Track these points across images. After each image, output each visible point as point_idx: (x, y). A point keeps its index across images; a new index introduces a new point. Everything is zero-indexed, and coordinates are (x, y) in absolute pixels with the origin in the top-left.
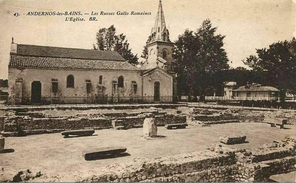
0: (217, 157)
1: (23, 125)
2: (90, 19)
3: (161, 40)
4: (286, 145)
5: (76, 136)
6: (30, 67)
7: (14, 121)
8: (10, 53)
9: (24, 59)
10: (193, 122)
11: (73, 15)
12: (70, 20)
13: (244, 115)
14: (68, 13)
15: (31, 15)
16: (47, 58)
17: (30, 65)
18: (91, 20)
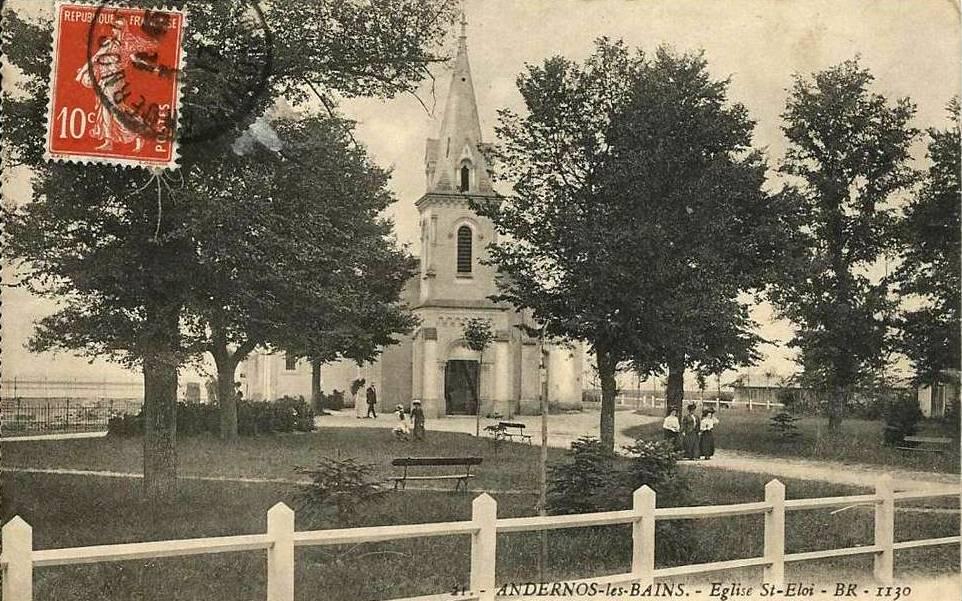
2: (633, 589)
7: (608, 121)
11: (657, 595)
12: (712, 595)
14: (642, 591)
15: (664, 595)
18: (635, 592)
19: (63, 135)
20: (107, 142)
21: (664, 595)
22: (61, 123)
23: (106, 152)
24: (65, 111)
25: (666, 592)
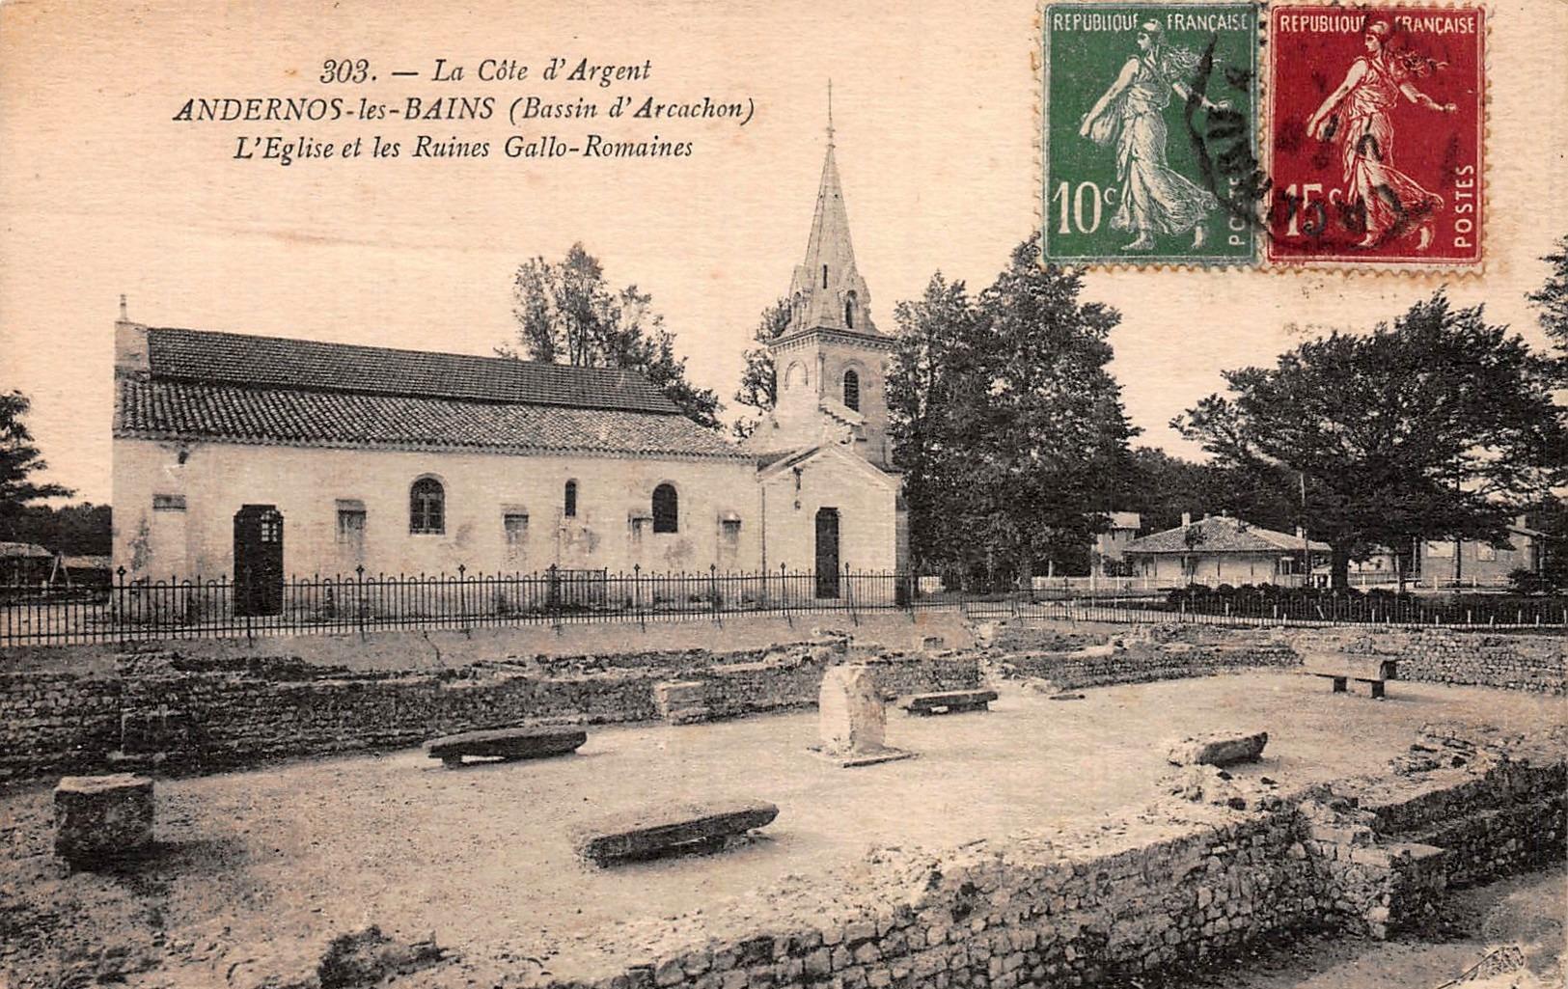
0: (1229, 824)
1: (219, 714)
3: (840, 324)
4: (1467, 759)
5: (496, 758)
6: (224, 436)
8: (113, 370)
9: (187, 399)
10: (1007, 682)
13: (1213, 649)
16: (303, 397)
17: (225, 427)
19: (1065, 229)
20: (1143, 236)
21: (461, 117)
22: (1060, 206)
23: (1145, 252)
24: (1064, 186)
25: (466, 111)
